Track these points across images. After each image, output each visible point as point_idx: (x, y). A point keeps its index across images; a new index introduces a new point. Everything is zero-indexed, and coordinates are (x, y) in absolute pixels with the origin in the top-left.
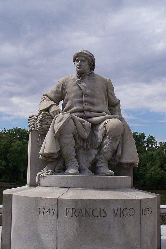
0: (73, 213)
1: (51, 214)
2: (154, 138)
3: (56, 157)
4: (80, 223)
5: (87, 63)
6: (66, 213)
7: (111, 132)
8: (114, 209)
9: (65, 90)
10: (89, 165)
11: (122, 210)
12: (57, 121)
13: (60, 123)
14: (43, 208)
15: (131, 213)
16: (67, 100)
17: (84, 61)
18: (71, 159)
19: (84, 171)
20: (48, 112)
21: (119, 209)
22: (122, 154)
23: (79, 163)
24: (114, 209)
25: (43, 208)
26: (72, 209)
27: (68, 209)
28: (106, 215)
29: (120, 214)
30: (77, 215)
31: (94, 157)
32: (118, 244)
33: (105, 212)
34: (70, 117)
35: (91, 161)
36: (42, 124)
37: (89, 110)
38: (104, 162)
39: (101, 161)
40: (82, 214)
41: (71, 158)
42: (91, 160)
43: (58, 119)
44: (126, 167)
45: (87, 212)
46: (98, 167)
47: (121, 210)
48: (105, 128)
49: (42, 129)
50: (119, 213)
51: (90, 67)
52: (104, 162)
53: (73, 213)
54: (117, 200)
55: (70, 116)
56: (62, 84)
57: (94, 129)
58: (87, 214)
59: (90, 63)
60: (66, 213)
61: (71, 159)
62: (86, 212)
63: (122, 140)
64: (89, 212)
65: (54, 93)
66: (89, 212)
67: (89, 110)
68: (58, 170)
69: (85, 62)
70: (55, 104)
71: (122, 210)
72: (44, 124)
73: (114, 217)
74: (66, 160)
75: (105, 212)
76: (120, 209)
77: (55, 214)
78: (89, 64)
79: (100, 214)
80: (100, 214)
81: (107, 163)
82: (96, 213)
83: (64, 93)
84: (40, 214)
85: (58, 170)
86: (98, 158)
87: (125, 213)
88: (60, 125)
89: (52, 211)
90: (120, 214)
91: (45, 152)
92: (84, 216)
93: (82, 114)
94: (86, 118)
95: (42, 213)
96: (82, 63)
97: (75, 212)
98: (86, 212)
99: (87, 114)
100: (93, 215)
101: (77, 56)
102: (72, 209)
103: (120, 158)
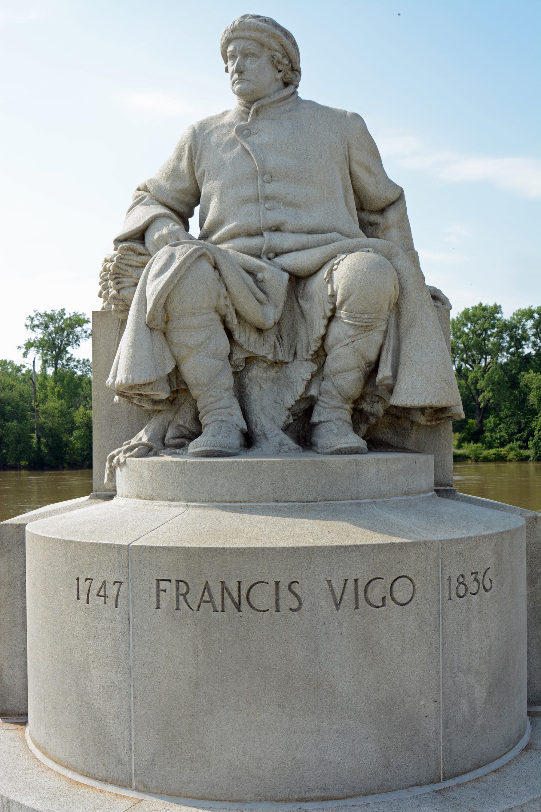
0: (181, 598)
1: (111, 600)
2: (532, 306)
3: (163, 395)
5: (265, 58)
6: (158, 596)
7: (351, 299)
8: (329, 582)
9: (199, 165)
10: (283, 417)
11: (362, 584)
12: (155, 269)
13: (161, 277)
14: (87, 579)
15: (401, 595)
16: (209, 199)
17: (253, 55)
19: (266, 439)
20: (144, 244)
21: (351, 584)
22: (395, 376)
23: (245, 415)
24: (472, 574)
25: (87, 579)
26: (178, 581)
27: (163, 585)
28: (300, 604)
29: (357, 599)
33: (296, 595)
34: (198, 254)
36: (120, 286)
38: (335, 407)
39: (323, 402)
40: (211, 601)
42: (290, 401)
43: (156, 264)
44: (422, 420)
45: (230, 595)
46: (315, 425)
47: (360, 583)
48: (329, 286)
49: (121, 303)
50: (349, 595)
51: (279, 76)
52: (335, 407)
53: (181, 598)
54: (298, 549)
55: (195, 251)
56: (187, 146)
57: (301, 291)
58: (228, 600)
59: (279, 62)
60: (158, 596)
62: (226, 594)
63: (398, 326)
64: (235, 594)
65: (167, 179)
66: (235, 594)
68: (176, 441)
69: (259, 57)
70: (164, 216)
71: (362, 584)
72: (127, 285)
74: (199, 406)
75: (296, 595)
78: (276, 65)
79: (277, 600)
80: (277, 600)
81: (345, 409)
83: (197, 175)
85: (176, 441)
86: (313, 392)
87: (375, 595)
88: (158, 284)
89: (112, 590)
90: (357, 599)
91: (119, 379)
92: (219, 608)
93: (255, 242)
94: (271, 255)
95: (83, 596)
96: (248, 62)
97: (187, 593)
98: (226, 594)
100: (249, 603)
101: (228, 41)
102: (178, 581)
103: (391, 390)
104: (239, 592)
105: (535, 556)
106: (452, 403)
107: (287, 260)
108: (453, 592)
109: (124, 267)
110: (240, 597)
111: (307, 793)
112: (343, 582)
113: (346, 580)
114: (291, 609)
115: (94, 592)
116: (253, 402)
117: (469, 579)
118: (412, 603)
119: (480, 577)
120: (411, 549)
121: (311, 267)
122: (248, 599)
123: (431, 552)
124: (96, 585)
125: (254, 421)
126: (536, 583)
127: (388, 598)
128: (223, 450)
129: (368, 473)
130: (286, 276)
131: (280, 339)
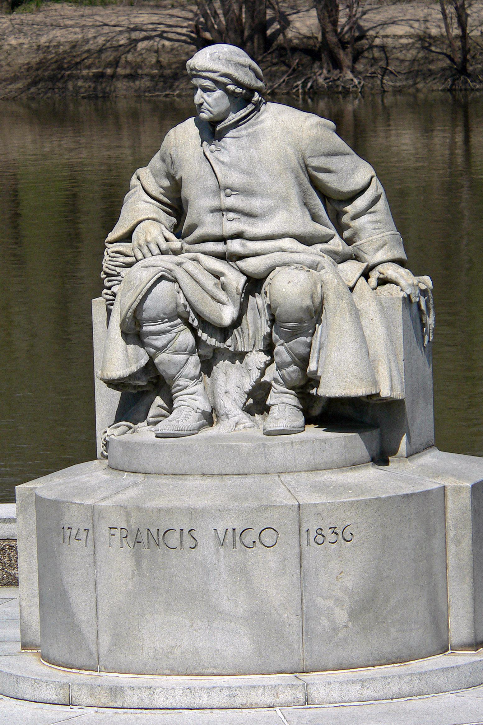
4: (138, 564)
11: (238, 532)
14: (69, 528)
18: (179, 388)
21: (230, 532)
30: (131, 545)
31: (256, 374)
32: (231, 614)
35: (247, 390)
37: (239, 236)
41: (179, 385)
47: (236, 531)
61: (179, 388)
62: (151, 537)
64: (156, 538)
66: (156, 538)
67: (239, 236)
71: (238, 532)
73: (218, 550)
76: (234, 529)
77: (90, 543)
82: (173, 540)
84: (227, 529)
89: (83, 535)
92: (147, 548)
93: (219, 247)
98: (151, 537)
99: (235, 246)
104: (158, 535)
105: (459, 520)
106: (268, 419)
107: (250, 265)
108: (312, 540)
109: (113, 268)
110: (158, 539)
111: (204, 670)
112: (225, 530)
113: (227, 529)
114: (190, 548)
115: (73, 537)
116: (219, 386)
117: (327, 532)
118: (277, 544)
119: (339, 531)
120: (275, 509)
121: (307, 235)
122: (164, 540)
123: (292, 512)
124: (74, 532)
125: (219, 403)
126: (460, 543)
127: (258, 542)
128: (176, 432)
129: (275, 453)
130: (243, 279)
131: (241, 332)
